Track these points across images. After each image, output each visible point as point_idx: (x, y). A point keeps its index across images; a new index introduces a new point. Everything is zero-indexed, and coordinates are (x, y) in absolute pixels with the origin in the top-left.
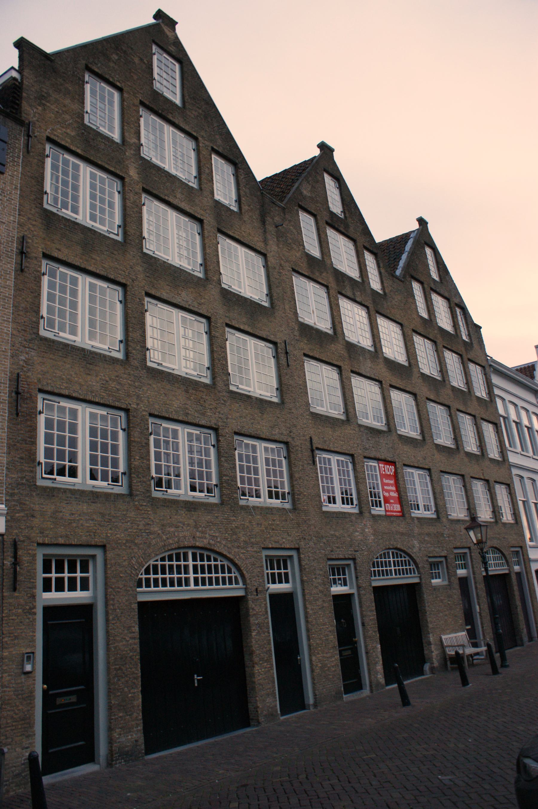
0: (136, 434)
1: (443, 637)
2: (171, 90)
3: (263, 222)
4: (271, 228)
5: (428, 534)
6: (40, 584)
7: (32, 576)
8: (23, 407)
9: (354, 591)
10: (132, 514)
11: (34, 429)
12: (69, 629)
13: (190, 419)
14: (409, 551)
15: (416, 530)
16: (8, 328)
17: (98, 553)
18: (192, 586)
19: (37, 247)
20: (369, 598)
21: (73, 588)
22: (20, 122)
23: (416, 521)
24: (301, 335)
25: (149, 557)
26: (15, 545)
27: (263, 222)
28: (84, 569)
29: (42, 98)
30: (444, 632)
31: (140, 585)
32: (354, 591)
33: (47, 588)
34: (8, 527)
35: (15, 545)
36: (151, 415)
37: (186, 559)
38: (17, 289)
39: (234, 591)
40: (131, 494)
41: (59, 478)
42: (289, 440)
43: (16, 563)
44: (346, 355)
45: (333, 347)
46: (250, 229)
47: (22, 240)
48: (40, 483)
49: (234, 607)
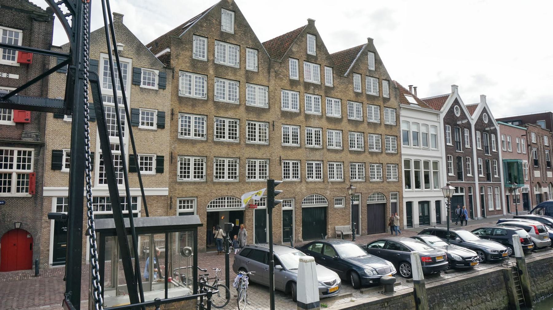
0: (209, 164)
1: (336, 227)
2: (312, 50)
3: (269, 73)
4: (273, 74)
5: (336, 188)
6: (178, 207)
7: (175, 205)
8: (173, 161)
9: (294, 209)
10: (206, 187)
11: (176, 166)
12: (355, 208)
13: (229, 156)
14: (324, 195)
15: (329, 187)
16: (169, 138)
17: (196, 199)
18: (226, 207)
19: (176, 110)
20: (300, 212)
21: (261, 205)
22: (171, 69)
23: (330, 184)
24: (281, 117)
25: (211, 199)
26: (171, 198)
27: (269, 73)
28: (192, 202)
29: (177, 56)
30: (337, 225)
31: (208, 207)
32: (294, 209)
33: (180, 207)
34: (169, 194)
35: (171, 198)
36: (215, 157)
37: (225, 199)
38: (171, 126)
39: (384, 202)
40: (324, 182)
41: (184, 179)
42: (270, 158)
43: (171, 203)
44: (304, 120)
45: (363, 126)
46: (261, 78)
47: (172, 110)
48: (178, 181)
49: (384, 205)
